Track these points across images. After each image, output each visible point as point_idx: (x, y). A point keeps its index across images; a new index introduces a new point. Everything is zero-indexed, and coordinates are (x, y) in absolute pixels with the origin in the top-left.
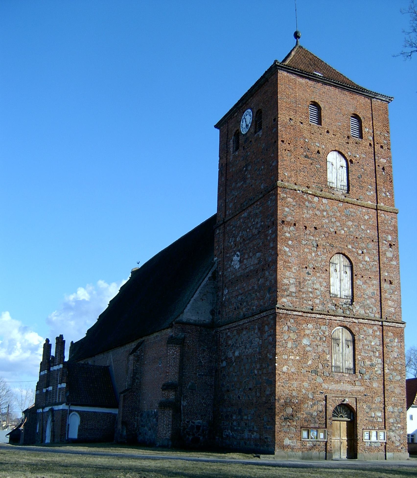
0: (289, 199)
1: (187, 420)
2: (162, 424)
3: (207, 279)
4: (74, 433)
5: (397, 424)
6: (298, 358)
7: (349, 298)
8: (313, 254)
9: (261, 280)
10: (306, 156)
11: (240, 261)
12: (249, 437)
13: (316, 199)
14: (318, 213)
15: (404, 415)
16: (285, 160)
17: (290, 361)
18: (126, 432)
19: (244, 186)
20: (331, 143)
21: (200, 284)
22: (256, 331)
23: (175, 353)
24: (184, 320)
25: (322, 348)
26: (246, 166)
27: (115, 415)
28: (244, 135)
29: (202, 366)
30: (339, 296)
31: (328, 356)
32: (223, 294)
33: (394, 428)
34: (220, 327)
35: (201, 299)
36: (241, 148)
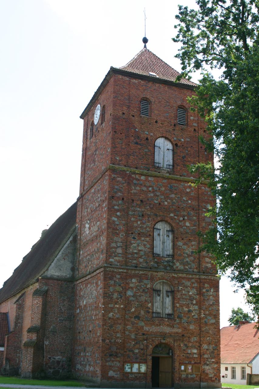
0: (118, 179)
1: (49, 356)
2: (26, 360)
3: (68, 242)
5: (212, 359)
6: (122, 306)
7: (170, 257)
8: (139, 223)
9: (99, 244)
10: (137, 143)
11: (89, 228)
13: (143, 178)
14: (144, 189)
15: (218, 352)
16: (117, 147)
17: (116, 309)
18: (9, 366)
19: (94, 167)
20: (159, 131)
21: (63, 246)
22: (94, 285)
23: (39, 302)
24: (49, 276)
25: (145, 298)
26: (96, 151)
28: (96, 126)
29: (62, 313)
30: (161, 256)
31: (150, 305)
33: (208, 363)
35: (63, 258)
36: (94, 136)
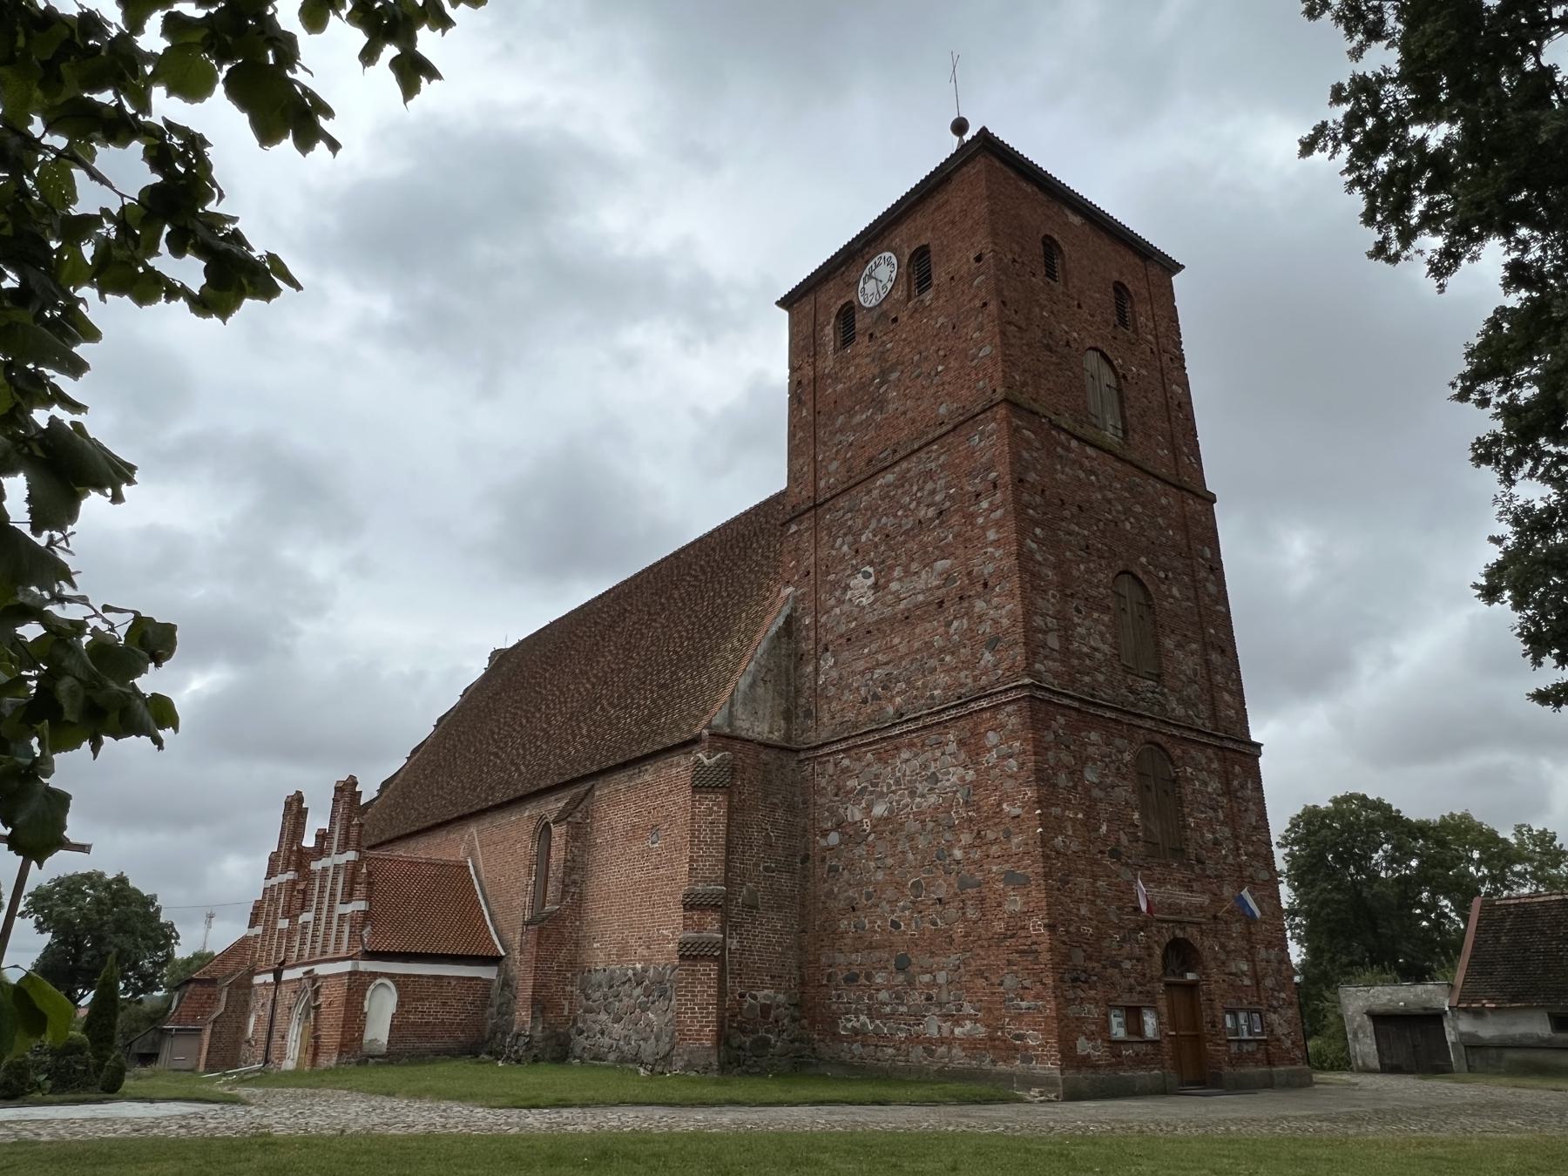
4: (378, 1031)
12: (946, 1033)
17: (1069, 824)
19: (879, 418)
26: (884, 374)
27: (488, 983)
32: (817, 670)
34: (170, 1007)
